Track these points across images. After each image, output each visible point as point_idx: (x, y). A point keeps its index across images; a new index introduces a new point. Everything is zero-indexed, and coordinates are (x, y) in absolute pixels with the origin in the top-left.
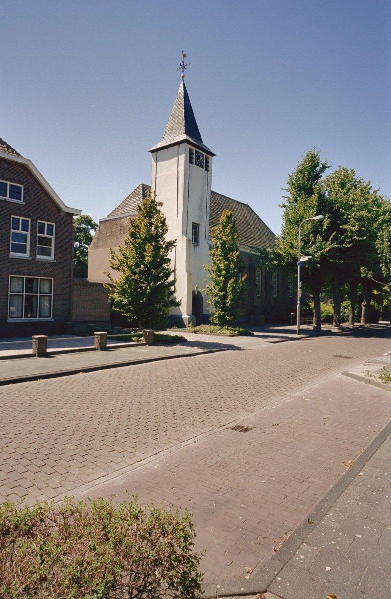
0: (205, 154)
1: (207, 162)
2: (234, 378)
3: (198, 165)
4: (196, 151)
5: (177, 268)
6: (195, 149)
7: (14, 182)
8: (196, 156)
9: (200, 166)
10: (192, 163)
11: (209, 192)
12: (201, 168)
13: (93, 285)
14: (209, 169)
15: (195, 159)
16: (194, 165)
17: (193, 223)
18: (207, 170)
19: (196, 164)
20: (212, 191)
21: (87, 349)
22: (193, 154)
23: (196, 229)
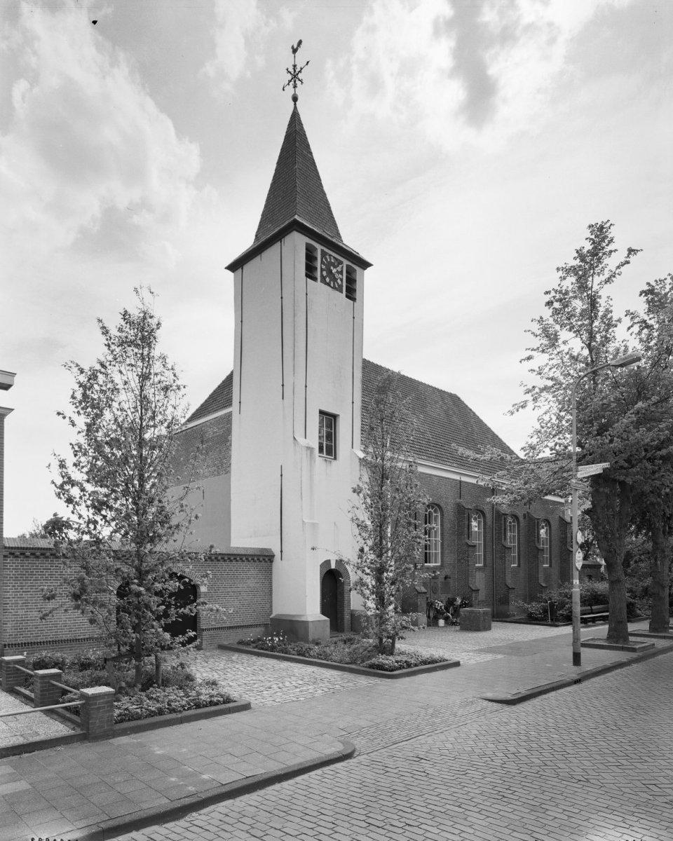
0: (346, 262)
1: (351, 281)
2: (360, 784)
3: (328, 284)
4: (322, 251)
5: (573, 521)
6: (319, 247)
7: (216, 411)
8: (322, 262)
9: (334, 288)
10: (315, 279)
11: (358, 366)
12: (338, 293)
13: (230, 710)
14: (358, 295)
15: (322, 270)
16: (318, 285)
17: (321, 412)
18: (351, 293)
19: (323, 280)
20: (364, 361)
21: (385, 674)
22: (316, 258)
23: (329, 426)
